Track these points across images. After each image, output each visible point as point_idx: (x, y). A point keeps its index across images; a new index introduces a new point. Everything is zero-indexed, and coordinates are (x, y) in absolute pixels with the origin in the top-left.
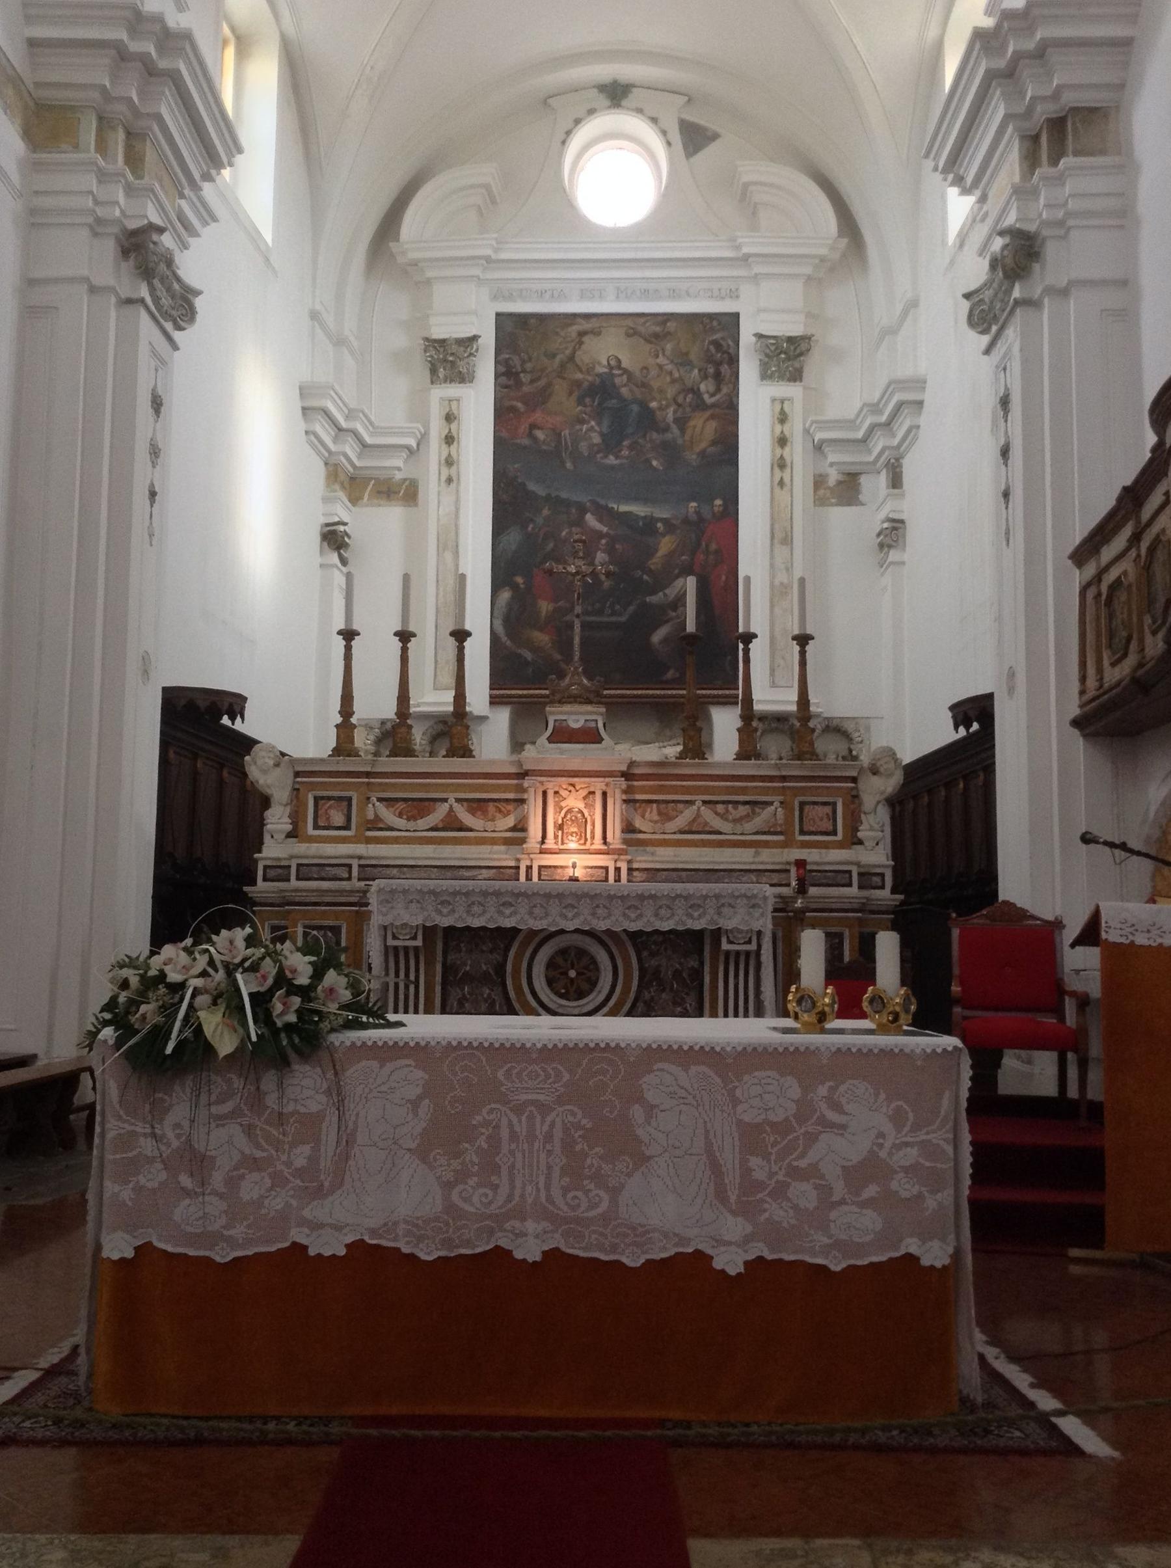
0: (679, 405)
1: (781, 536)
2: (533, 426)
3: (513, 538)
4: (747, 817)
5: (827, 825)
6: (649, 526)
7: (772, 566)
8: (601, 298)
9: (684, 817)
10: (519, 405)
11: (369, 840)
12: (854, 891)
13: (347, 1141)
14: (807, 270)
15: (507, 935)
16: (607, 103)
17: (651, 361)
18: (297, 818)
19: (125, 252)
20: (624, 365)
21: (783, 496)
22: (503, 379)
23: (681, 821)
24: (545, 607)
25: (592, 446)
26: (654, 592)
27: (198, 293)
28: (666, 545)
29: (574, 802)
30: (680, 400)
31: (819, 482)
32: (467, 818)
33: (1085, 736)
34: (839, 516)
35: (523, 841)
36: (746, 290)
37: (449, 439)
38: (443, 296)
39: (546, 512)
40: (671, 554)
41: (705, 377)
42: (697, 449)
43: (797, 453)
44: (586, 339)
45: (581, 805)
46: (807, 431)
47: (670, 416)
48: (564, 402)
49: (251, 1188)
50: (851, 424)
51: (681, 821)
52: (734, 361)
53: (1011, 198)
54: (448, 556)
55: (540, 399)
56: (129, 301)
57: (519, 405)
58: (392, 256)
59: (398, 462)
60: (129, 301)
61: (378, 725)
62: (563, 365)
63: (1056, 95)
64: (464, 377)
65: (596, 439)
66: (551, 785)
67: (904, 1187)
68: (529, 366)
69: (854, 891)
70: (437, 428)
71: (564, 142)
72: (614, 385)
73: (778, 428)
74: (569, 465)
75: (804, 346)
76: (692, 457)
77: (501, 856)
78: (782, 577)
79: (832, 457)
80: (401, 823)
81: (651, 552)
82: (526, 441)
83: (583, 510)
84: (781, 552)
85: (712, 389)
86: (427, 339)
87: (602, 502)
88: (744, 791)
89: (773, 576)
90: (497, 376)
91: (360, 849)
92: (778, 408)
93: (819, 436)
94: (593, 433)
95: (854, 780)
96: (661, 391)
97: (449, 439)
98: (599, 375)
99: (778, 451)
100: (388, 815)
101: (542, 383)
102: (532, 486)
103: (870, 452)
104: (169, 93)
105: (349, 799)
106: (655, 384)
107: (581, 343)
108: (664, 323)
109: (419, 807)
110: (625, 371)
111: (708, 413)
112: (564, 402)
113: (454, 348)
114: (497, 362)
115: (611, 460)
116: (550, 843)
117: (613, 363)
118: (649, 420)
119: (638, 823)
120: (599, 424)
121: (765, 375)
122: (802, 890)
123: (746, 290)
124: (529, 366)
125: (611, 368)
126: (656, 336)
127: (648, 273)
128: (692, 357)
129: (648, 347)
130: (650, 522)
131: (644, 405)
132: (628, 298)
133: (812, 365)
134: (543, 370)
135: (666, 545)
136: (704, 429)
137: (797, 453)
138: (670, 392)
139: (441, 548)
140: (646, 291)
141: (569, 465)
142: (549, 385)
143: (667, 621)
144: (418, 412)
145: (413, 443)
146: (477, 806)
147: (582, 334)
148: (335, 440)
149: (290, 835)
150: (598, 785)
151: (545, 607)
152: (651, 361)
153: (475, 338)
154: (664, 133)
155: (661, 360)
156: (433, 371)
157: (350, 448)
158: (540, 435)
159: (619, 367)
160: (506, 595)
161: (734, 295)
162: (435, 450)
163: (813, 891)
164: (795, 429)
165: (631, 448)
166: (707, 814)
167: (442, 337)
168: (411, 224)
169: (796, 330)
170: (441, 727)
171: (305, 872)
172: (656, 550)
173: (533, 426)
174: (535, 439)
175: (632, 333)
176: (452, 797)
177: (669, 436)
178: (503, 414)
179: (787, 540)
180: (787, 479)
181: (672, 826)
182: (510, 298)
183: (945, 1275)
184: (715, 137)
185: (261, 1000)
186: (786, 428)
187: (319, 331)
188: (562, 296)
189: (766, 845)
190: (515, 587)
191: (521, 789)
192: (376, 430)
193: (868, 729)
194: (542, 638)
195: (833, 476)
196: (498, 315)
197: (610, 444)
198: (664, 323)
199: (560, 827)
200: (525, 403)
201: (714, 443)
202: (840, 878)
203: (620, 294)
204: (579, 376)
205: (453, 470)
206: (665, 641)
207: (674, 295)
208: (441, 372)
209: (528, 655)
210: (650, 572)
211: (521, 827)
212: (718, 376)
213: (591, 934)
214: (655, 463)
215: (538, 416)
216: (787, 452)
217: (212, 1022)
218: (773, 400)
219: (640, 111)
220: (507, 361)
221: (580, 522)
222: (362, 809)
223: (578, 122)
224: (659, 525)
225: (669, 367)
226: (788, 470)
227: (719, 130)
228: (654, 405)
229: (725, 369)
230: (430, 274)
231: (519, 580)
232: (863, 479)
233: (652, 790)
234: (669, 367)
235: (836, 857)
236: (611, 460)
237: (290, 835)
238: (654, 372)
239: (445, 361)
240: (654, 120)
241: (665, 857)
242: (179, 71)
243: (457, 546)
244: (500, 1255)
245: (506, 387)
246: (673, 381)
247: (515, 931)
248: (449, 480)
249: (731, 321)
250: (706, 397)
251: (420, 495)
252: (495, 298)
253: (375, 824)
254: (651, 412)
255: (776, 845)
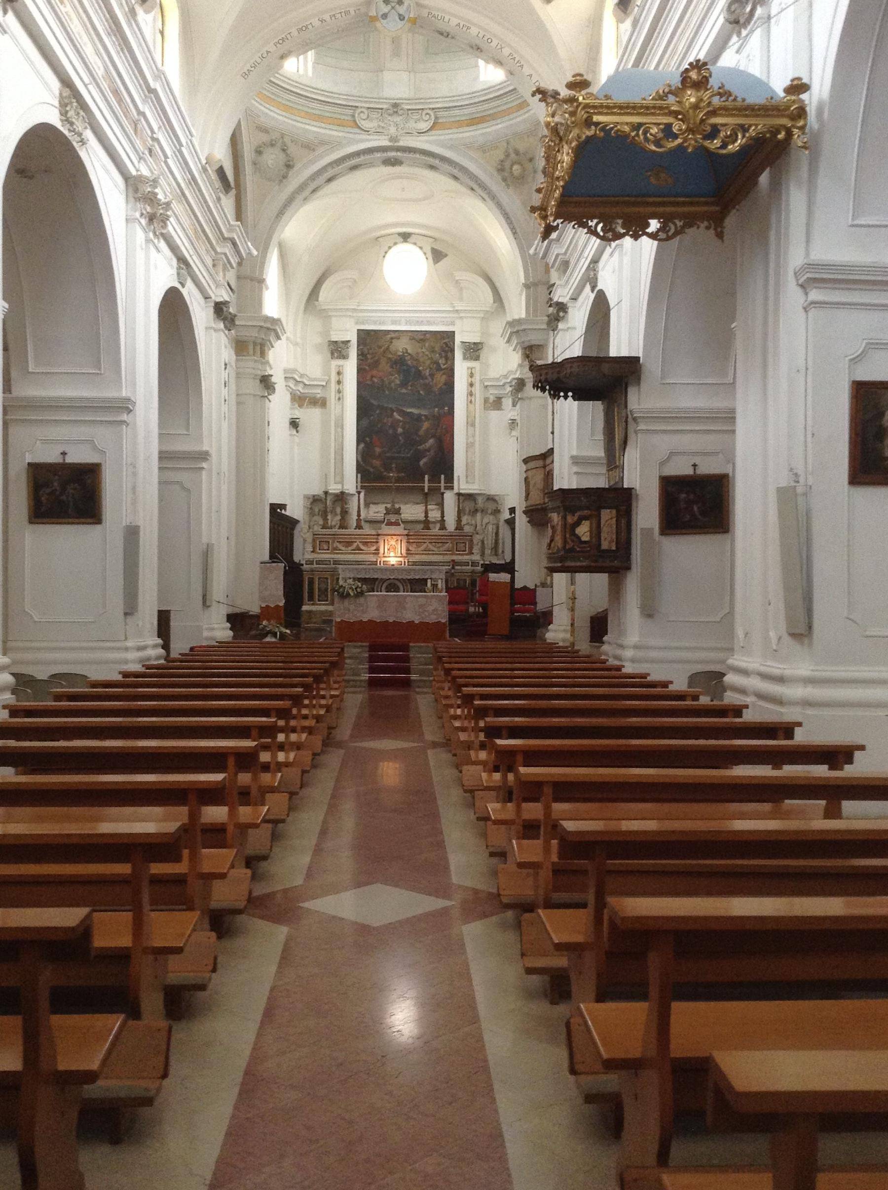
0: (431, 368)
1: (470, 423)
2: (372, 377)
3: (365, 422)
4: (442, 546)
5: (463, 549)
6: (418, 418)
7: (467, 435)
8: (400, 324)
9: (424, 546)
10: (367, 368)
11: (335, 553)
12: (470, 567)
13: (367, 607)
14: (482, 315)
15: (375, 580)
16: (402, 240)
17: (420, 350)
18: (314, 547)
19: (261, 381)
20: (409, 351)
21: (471, 407)
22: (360, 357)
23: (422, 548)
24: (378, 450)
25: (396, 385)
26: (421, 445)
27: (275, 384)
28: (426, 425)
29: (393, 542)
30: (431, 366)
31: (486, 400)
32: (362, 547)
33: (532, 525)
34: (494, 414)
35: (378, 553)
36: (458, 322)
37: (339, 382)
38: (336, 323)
39: (378, 412)
40: (427, 429)
41: (441, 357)
42: (438, 387)
43: (477, 389)
44: (393, 341)
45: (394, 543)
46: (481, 381)
47: (427, 374)
48: (385, 366)
49: (356, 613)
50: (497, 379)
51: (422, 548)
52: (452, 351)
53: (719, 15)
54: (339, 430)
55: (376, 364)
56: (262, 397)
57: (367, 368)
58: (316, 306)
59: (319, 391)
60: (262, 397)
61: (311, 497)
62: (384, 352)
63: (529, 341)
64: (345, 357)
65: (398, 382)
66: (386, 538)
67: (439, 612)
68: (370, 351)
69: (470, 567)
70: (334, 378)
71: (384, 257)
72: (405, 360)
73: (470, 380)
74: (387, 392)
75: (480, 346)
76: (436, 389)
77: (372, 558)
78: (471, 440)
79: (492, 391)
80: (343, 548)
81: (418, 430)
82: (369, 382)
83: (392, 411)
84: (471, 429)
85: (444, 362)
86: (329, 341)
87: (400, 408)
88: (442, 539)
89: (467, 439)
90: (358, 355)
91: (333, 556)
92: (470, 370)
93: (486, 384)
94: (397, 379)
95: (471, 536)
96: (424, 363)
97: (339, 382)
98: (399, 356)
99: (470, 389)
100: (340, 546)
101: (376, 358)
102: (373, 401)
103: (505, 389)
104: (273, 333)
105: (329, 542)
106: (421, 360)
107: (391, 342)
108: (425, 335)
109: (349, 544)
110: (409, 354)
111: (442, 372)
112: (385, 366)
113: (341, 345)
114: (358, 350)
115: (404, 391)
116: (386, 555)
117: (404, 351)
118: (419, 374)
119: (410, 548)
120: (399, 376)
121: (465, 358)
122: (453, 568)
123: (458, 322)
124: (370, 351)
125: (404, 353)
126: (421, 340)
127: (417, 315)
128: (436, 349)
129: (418, 344)
130: (420, 415)
131: (417, 368)
132: (410, 324)
133: (483, 354)
134: (376, 353)
135: (426, 425)
136: (441, 379)
137: (477, 389)
138: (428, 362)
139: (336, 426)
140: (418, 321)
141: (387, 392)
142: (379, 359)
143: (425, 457)
144: (327, 372)
145: (324, 384)
146: (365, 544)
147: (392, 338)
148: (295, 385)
149: (313, 552)
150: (399, 538)
151: (378, 450)
152: (420, 350)
153: (349, 341)
154: (425, 254)
155: (423, 350)
156: (332, 354)
157: (300, 388)
158: (375, 380)
159: (407, 352)
160: (362, 445)
161: (453, 323)
162: (333, 386)
163: (456, 567)
164: (477, 379)
165: (411, 386)
166: (430, 546)
167: (335, 340)
168: (323, 294)
169: (477, 340)
170: (336, 498)
171: (318, 563)
172: (422, 428)
173: (372, 377)
174: (373, 382)
175: (412, 339)
176: (358, 541)
177: (427, 381)
178: (360, 371)
179: (473, 425)
180: (473, 400)
181: (420, 549)
182: (363, 323)
183: (444, 624)
184: (446, 255)
185: (356, 589)
186: (473, 380)
187: (289, 344)
188: (383, 323)
189: (446, 554)
190: (366, 443)
191: (377, 539)
192: (310, 379)
193: (504, 499)
194: (377, 463)
195: (492, 398)
196: (358, 330)
197: (404, 384)
198: (425, 335)
199: (389, 550)
200: (369, 366)
201: (445, 384)
202: (466, 564)
203: (408, 322)
204: (390, 356)
205: (341, 394)
206: (425, 464)
207: (429, 323)
208: (336, 355)
209: (372, 470)
210: (419, 436)
211: (378, 549)
212: (447, 358)
213: (397, 579)
214: (421, 392)
215: (374, 372)
216: (473, 389)
217: (350, 591)
218: (468, 368)
219: (415, 244)
220: (362, 349)
221: (392, 416)
222: (332, 545)
223: (390, 248)
224: (423, 417)
225: (427, 353)
226: (473, 397)
227: (448, 253)
228: (421, 368)
229: (449, 354)
230: (330, 314)
231: (368, 439)
232: (503, 400)
233: (416, 539)
234: (427, 353)
235: (466, 558)
236: (404, 391)
237: (313, 552)
238: (421, 355)
239: (337, 350)
240: (421, 248)
241: (417, 558)
242: (234, 238)
243: (284, 272)
244: (387, 621)
245: (362, 360)
246: (429, 359)
247: (377, 579)
248: (339, 399)
249: (452, 334)
250: (442, 365)
251: (328, 403)
252: (357, 323)
253: (336, 549)
254: (420, 371)
255: (450, 554)
